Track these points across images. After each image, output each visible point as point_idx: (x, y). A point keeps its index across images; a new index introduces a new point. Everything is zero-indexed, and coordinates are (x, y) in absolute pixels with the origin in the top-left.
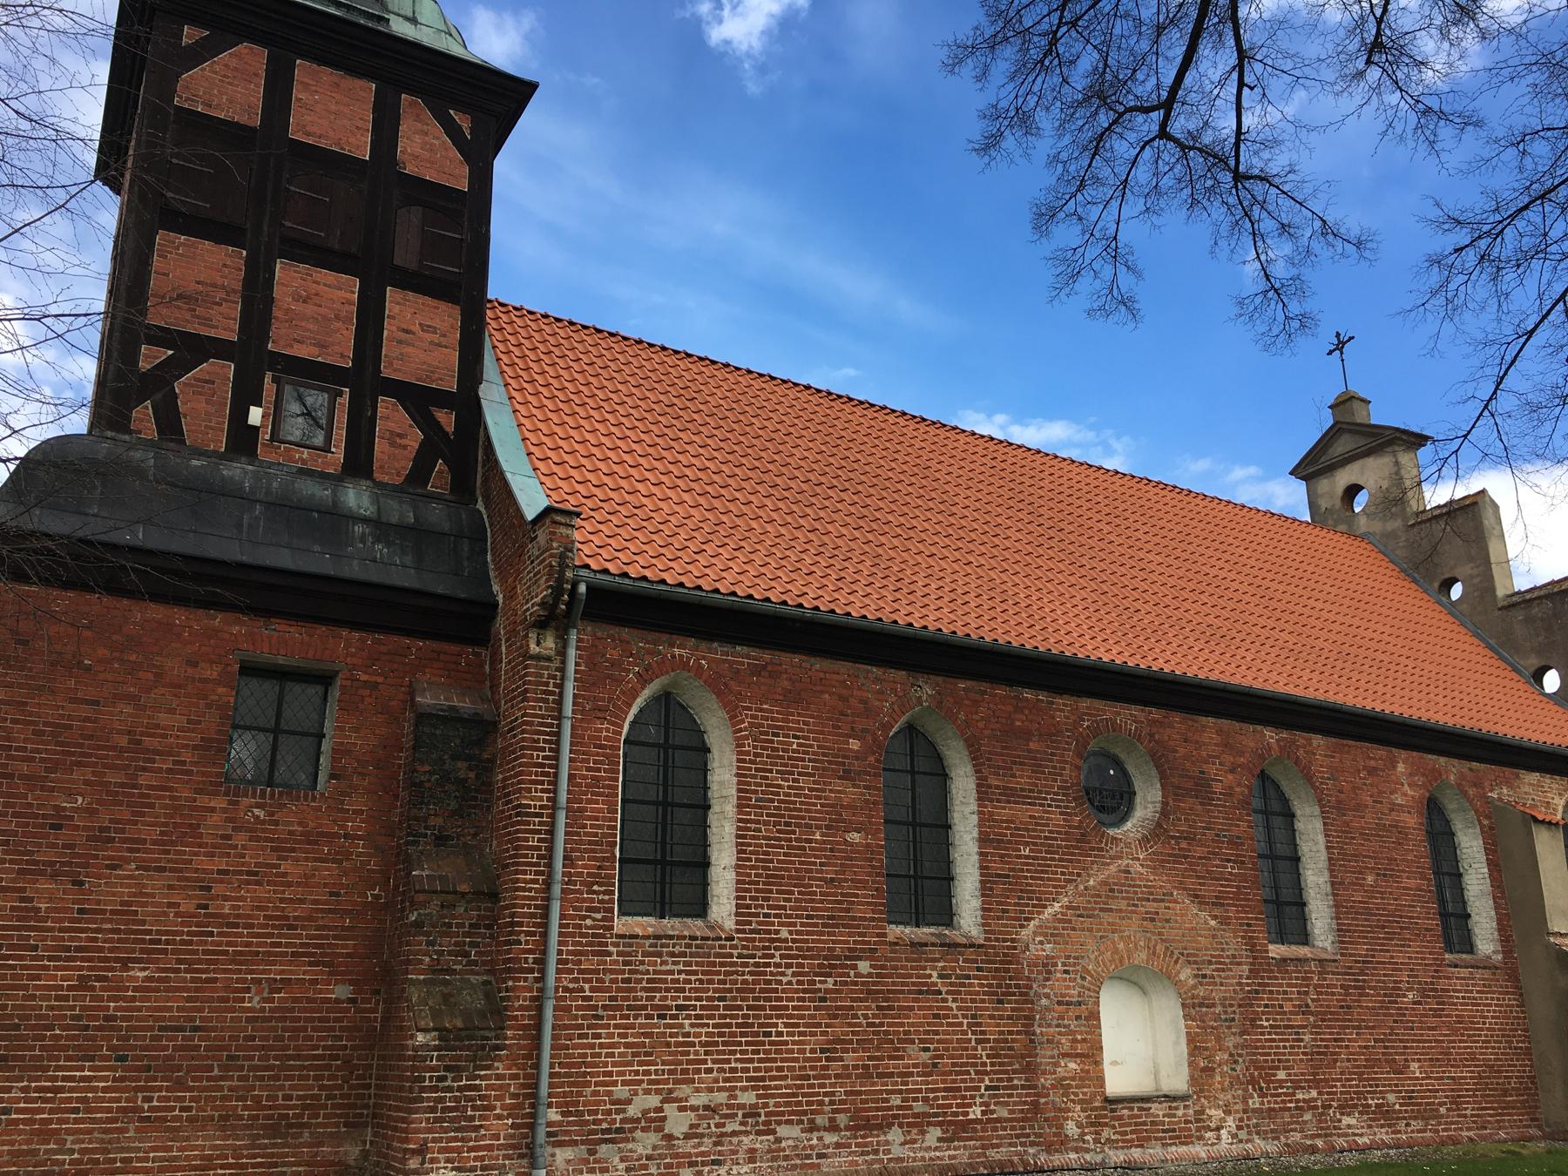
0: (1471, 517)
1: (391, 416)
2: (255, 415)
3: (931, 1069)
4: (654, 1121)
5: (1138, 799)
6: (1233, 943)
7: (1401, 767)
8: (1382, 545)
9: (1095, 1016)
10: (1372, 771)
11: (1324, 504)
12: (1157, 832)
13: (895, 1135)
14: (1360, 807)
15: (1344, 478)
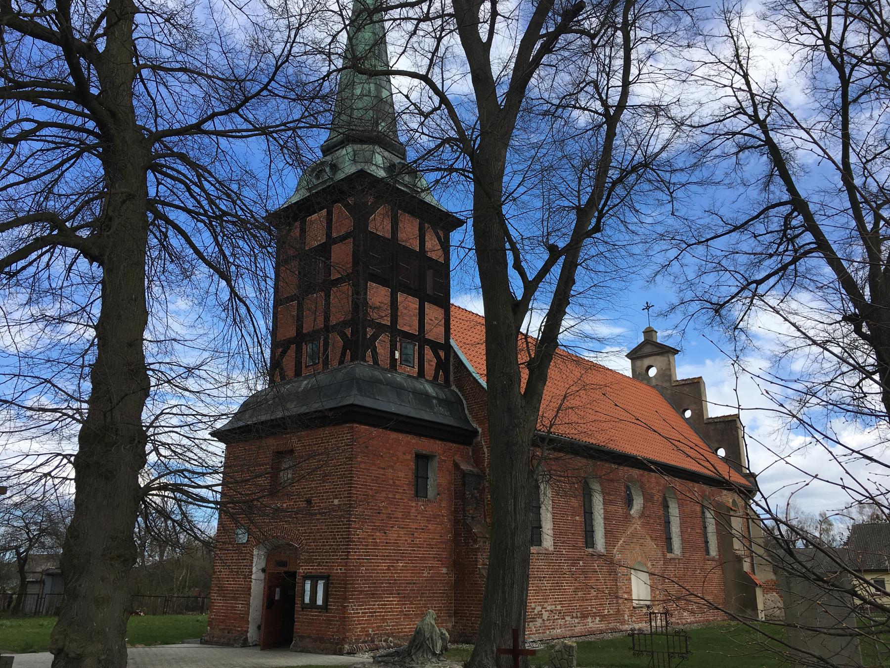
0: (695, 386)
3: (596, 597)
5: (634, 502)
6: (660, 554)
8: (662, 391)
9: (630, 579)
11: (638, 370)
12: (642, 515)
13: (590, 620)
15: (647, 362)
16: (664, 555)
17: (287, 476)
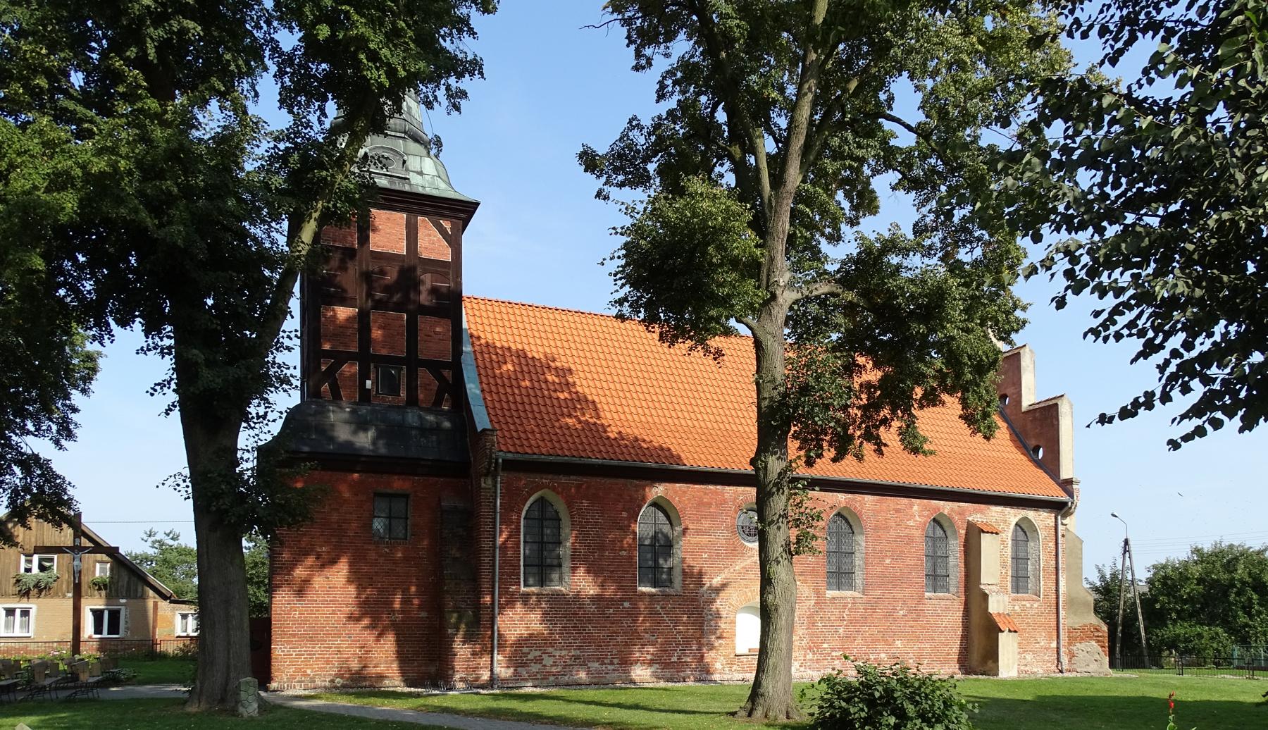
1: (424, 375)
2: (369, 383)
4: (538, 660)
7: (915, 508)
10: (897, 511)
14: (887, 528)
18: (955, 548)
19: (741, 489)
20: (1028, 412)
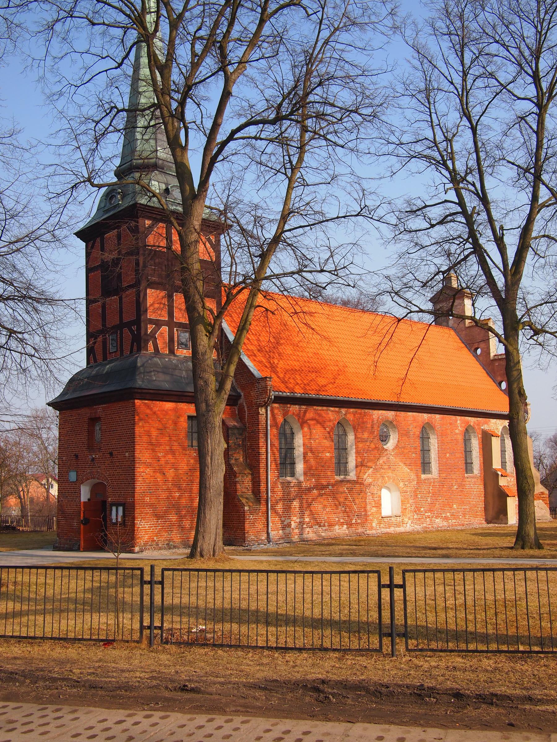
16: (418, 477)
17: (98, 435)
18: (475, 444)
19: (381, 412)
20: (494, 360)
